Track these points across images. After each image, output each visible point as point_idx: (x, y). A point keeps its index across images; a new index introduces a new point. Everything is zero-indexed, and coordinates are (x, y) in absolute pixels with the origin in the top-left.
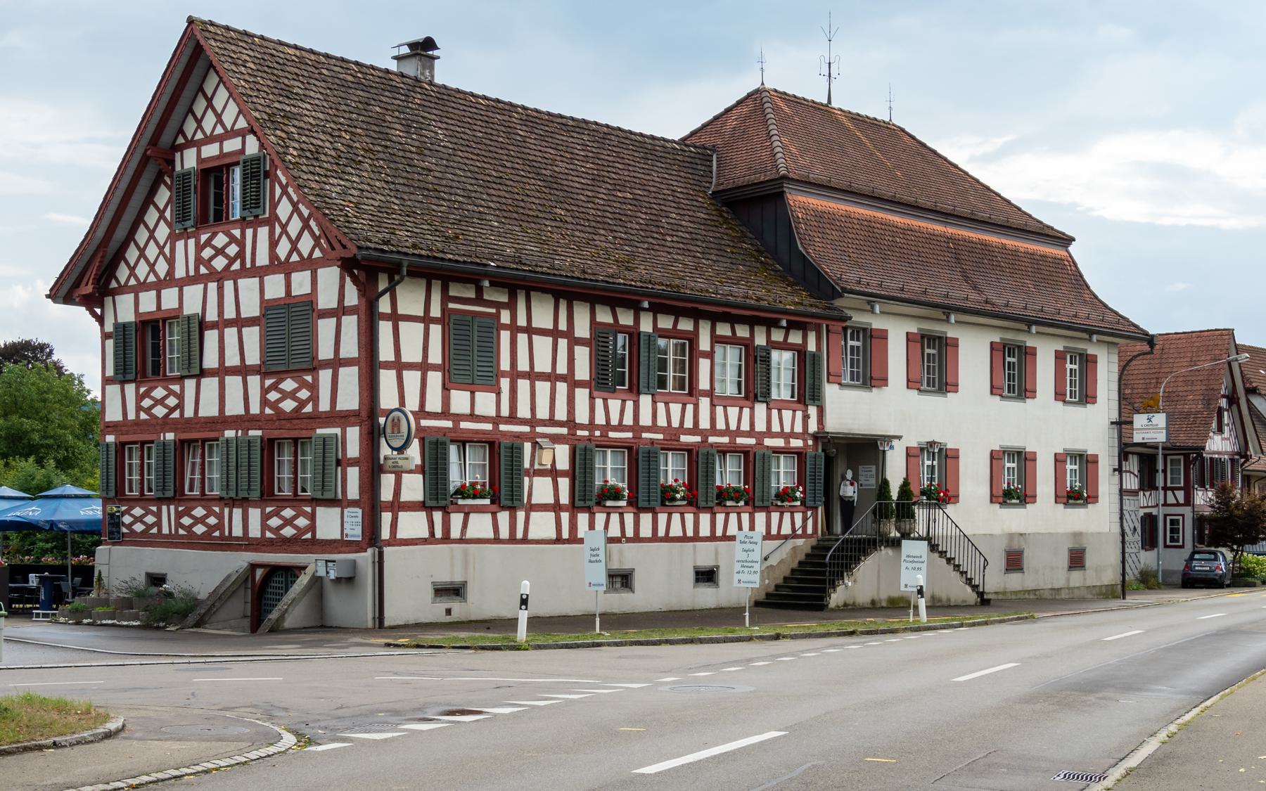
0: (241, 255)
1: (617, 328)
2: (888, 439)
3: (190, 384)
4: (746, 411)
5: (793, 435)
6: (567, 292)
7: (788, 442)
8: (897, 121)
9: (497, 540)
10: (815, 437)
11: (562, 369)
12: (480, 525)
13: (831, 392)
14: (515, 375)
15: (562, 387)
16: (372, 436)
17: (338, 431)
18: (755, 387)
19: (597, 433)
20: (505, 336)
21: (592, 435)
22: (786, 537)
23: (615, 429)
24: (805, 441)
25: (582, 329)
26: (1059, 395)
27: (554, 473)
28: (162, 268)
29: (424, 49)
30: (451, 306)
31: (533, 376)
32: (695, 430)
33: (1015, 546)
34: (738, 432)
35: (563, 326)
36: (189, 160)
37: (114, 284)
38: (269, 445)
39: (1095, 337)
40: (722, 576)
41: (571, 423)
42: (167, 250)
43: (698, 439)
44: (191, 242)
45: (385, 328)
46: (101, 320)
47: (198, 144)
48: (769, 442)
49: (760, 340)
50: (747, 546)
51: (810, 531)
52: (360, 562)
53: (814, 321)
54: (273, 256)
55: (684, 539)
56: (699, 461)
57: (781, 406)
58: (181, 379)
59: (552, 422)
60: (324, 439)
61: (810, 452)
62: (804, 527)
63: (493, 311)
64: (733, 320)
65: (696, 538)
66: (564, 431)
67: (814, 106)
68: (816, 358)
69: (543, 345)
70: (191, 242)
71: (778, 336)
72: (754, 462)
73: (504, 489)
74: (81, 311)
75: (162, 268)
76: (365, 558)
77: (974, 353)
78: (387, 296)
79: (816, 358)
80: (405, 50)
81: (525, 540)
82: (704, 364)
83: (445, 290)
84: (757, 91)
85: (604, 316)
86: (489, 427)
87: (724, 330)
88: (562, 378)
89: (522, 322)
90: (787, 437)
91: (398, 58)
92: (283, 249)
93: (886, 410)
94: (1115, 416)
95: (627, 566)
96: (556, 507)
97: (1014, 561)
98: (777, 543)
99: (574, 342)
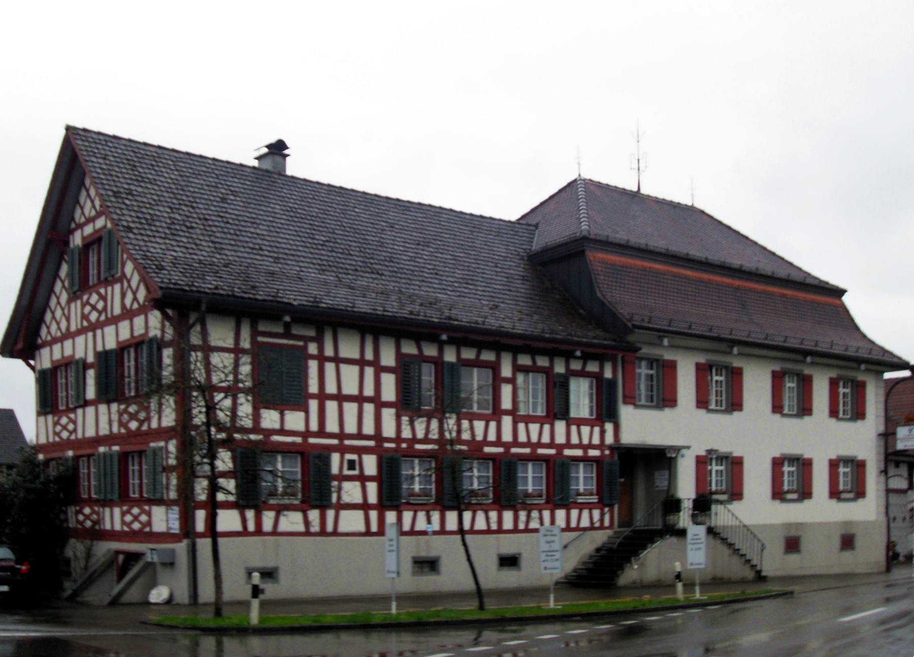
0: (105, 308)
1: (421, 358)
2: (677, 449)
3: (80, 411)
4: (547, 427)
5: (591, 446)
6: (373, 327)
7: (585, 452)
8: (699, 205)
9: (307, 533)
10: (611, 448)
11: (369, 391)
12: (292, 521)
13: (626, 412)
14: (322, 397)
15: (369, 408)
16: (186, 447)
17: (162, 444)
18: (558, 408)
19: (404, 445)
20: (313, 365)
21: (398, 446)
22: (585, 529)
23: (421, 442)
24: (602, 451)
25: (388, 358)
26: (834, 413)
27: (363, 479)
28: (64, 325)
29: (278, 149)
30: (260, 339)
31: (340, 398)
32: (498, 442)
33: (793, 533)
34: (540, 445)
35: (369, 356)
36: (77, 240)
37: (39, 341)
38: (124, 457)
39: (863, 367)
40: (524, 562)
41: (378, 436)
42: (66, 312)
43: (501, 450)
44: (79, 302)
45: (196, 357)
46: (33, 368)
47: (80, 226)
48: (567, 452)
49: (559, 368)
50: (549, 538)
51: (607, 523)
52: (178, 551)
53: (610, 352)
54: (123, 306)
55: (489, 531)
56: (505, 468)
57: (580, 422)
58: (74, 410)
59: (360, 436)
60: (155, 451)
61: (607, 460)
62: (602, 520)
63: (301, 343)
64: (534, 352)
65: (500, 531)
66: (372, 443)
67: (624, 192)
68: (612, 383)
69: (350, 374)
70: (79, 302)
71: (576, 365)
72: (558, 469)
73: (316, 491)
74: (19, 363)
75: (64, 325)
76: (181, 547)
77: (757, 382)
78: (198, 328)
79: (612, 383)
80: (266, 150)
81: (335, 533)
82: (506, 391)
83: (254, 326)
84: (575, 181)
85: (409, 348)
86: (299, 440)
87: (524, 360)
88: (369, 400)
89: (329, 351)
90: (585, 448)
91: (258, 158)
92: (128, 300)
93: (679, 427)
94: (882, 429)
95: (433, 554)
96: (365, 506)
97: (792, 545)
98: (574, 534)
99: (380, 370)
